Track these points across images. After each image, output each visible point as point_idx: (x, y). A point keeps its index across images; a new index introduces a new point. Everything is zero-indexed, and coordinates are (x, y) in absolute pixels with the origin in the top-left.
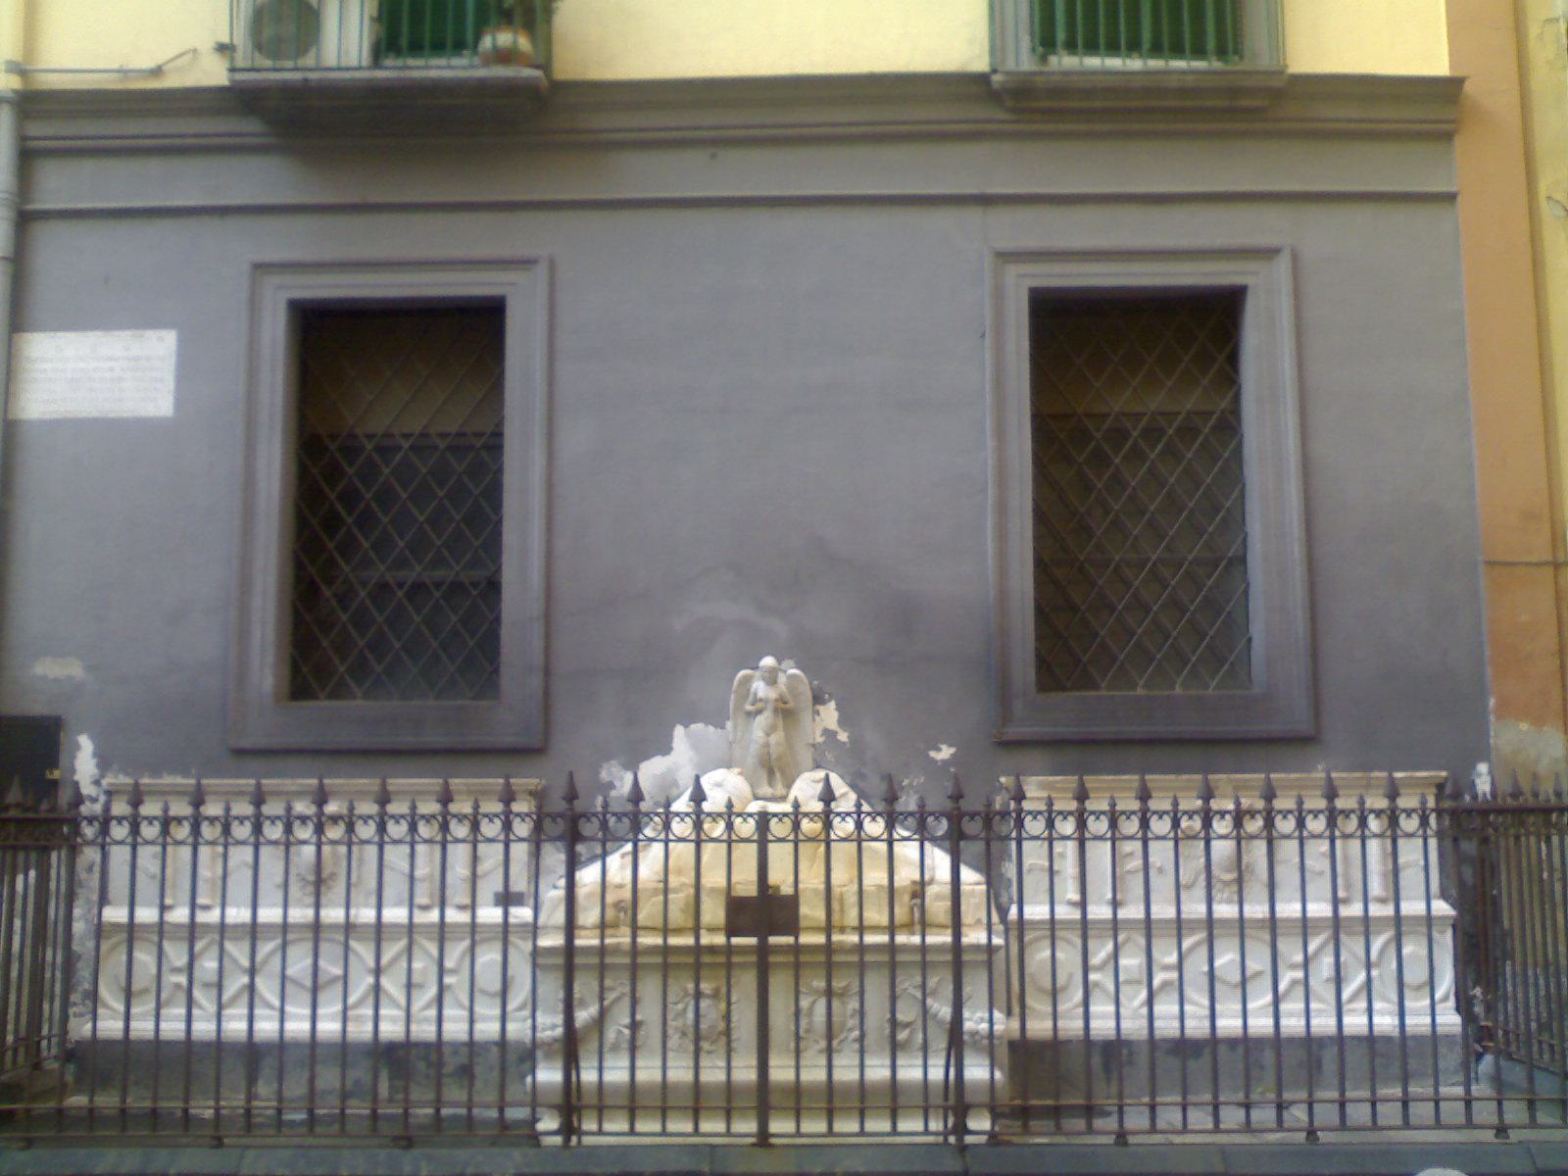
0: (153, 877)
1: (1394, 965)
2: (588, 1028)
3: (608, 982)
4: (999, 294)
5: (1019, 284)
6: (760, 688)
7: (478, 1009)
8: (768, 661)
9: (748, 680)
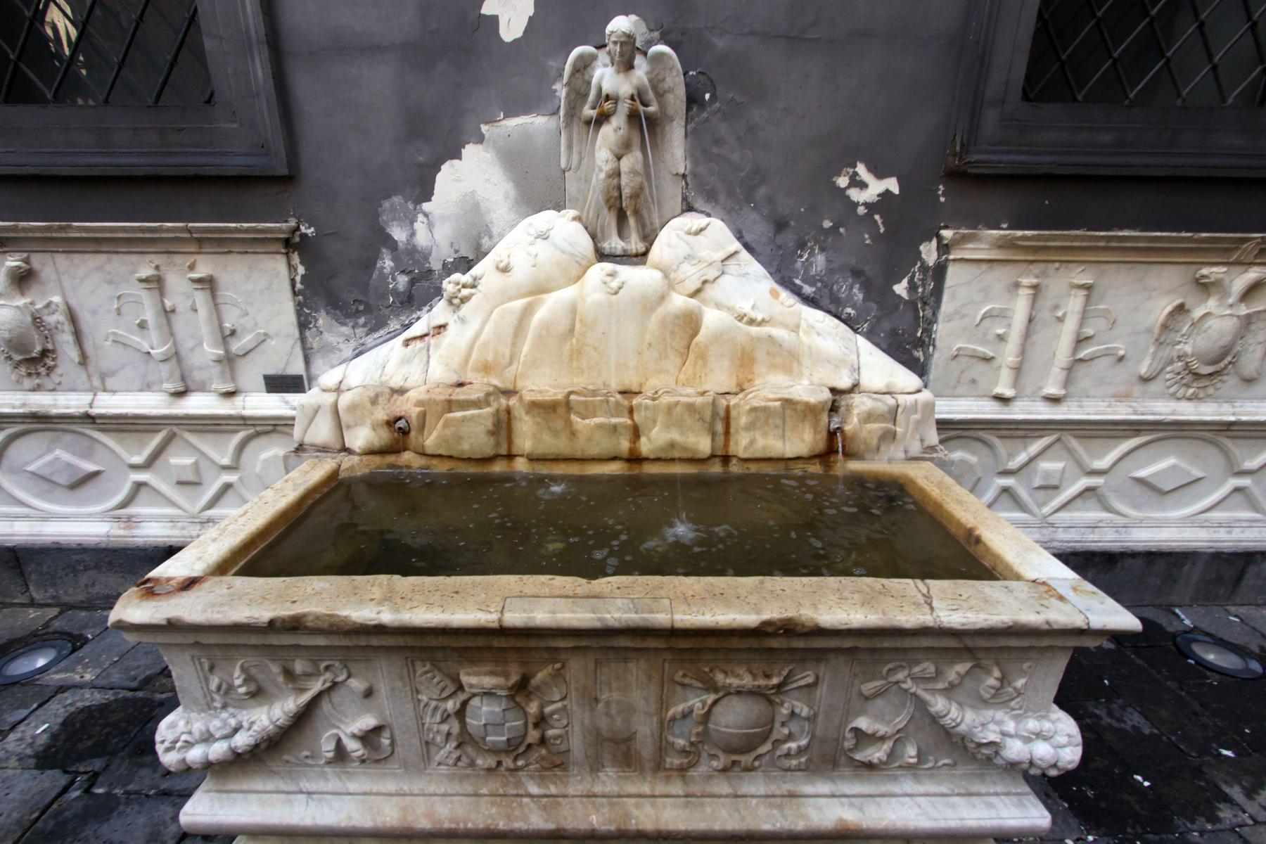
6: (605, 76)
8: (621, 24)
9: (584, 65)
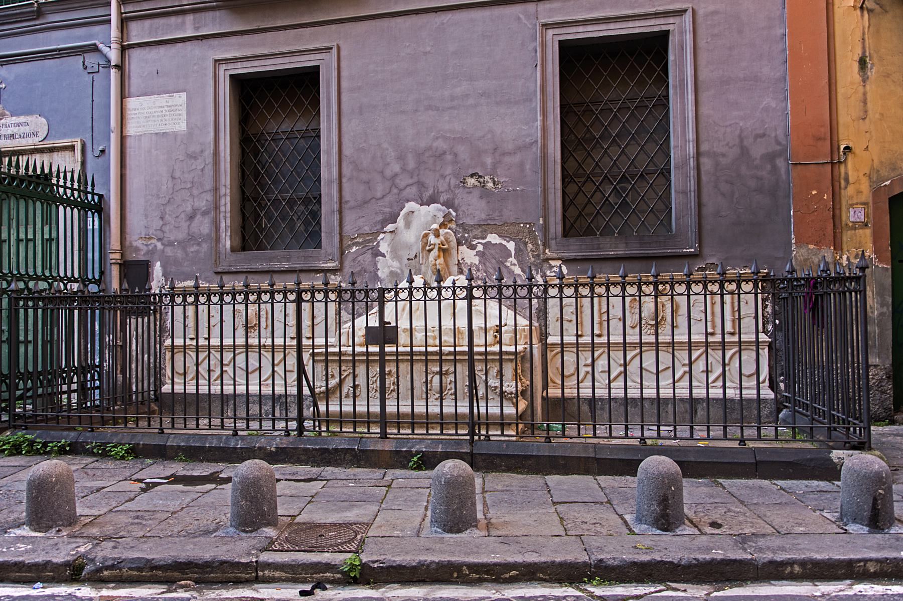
0: (620, 319)
1: (738, 365)
2: (335, 388)
3: (343, 368)
4: (544, 45)
5: (553, 38)
7: (175, 380)
